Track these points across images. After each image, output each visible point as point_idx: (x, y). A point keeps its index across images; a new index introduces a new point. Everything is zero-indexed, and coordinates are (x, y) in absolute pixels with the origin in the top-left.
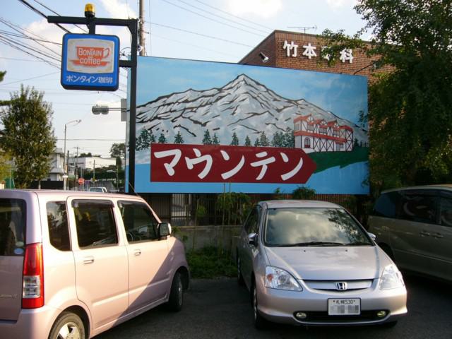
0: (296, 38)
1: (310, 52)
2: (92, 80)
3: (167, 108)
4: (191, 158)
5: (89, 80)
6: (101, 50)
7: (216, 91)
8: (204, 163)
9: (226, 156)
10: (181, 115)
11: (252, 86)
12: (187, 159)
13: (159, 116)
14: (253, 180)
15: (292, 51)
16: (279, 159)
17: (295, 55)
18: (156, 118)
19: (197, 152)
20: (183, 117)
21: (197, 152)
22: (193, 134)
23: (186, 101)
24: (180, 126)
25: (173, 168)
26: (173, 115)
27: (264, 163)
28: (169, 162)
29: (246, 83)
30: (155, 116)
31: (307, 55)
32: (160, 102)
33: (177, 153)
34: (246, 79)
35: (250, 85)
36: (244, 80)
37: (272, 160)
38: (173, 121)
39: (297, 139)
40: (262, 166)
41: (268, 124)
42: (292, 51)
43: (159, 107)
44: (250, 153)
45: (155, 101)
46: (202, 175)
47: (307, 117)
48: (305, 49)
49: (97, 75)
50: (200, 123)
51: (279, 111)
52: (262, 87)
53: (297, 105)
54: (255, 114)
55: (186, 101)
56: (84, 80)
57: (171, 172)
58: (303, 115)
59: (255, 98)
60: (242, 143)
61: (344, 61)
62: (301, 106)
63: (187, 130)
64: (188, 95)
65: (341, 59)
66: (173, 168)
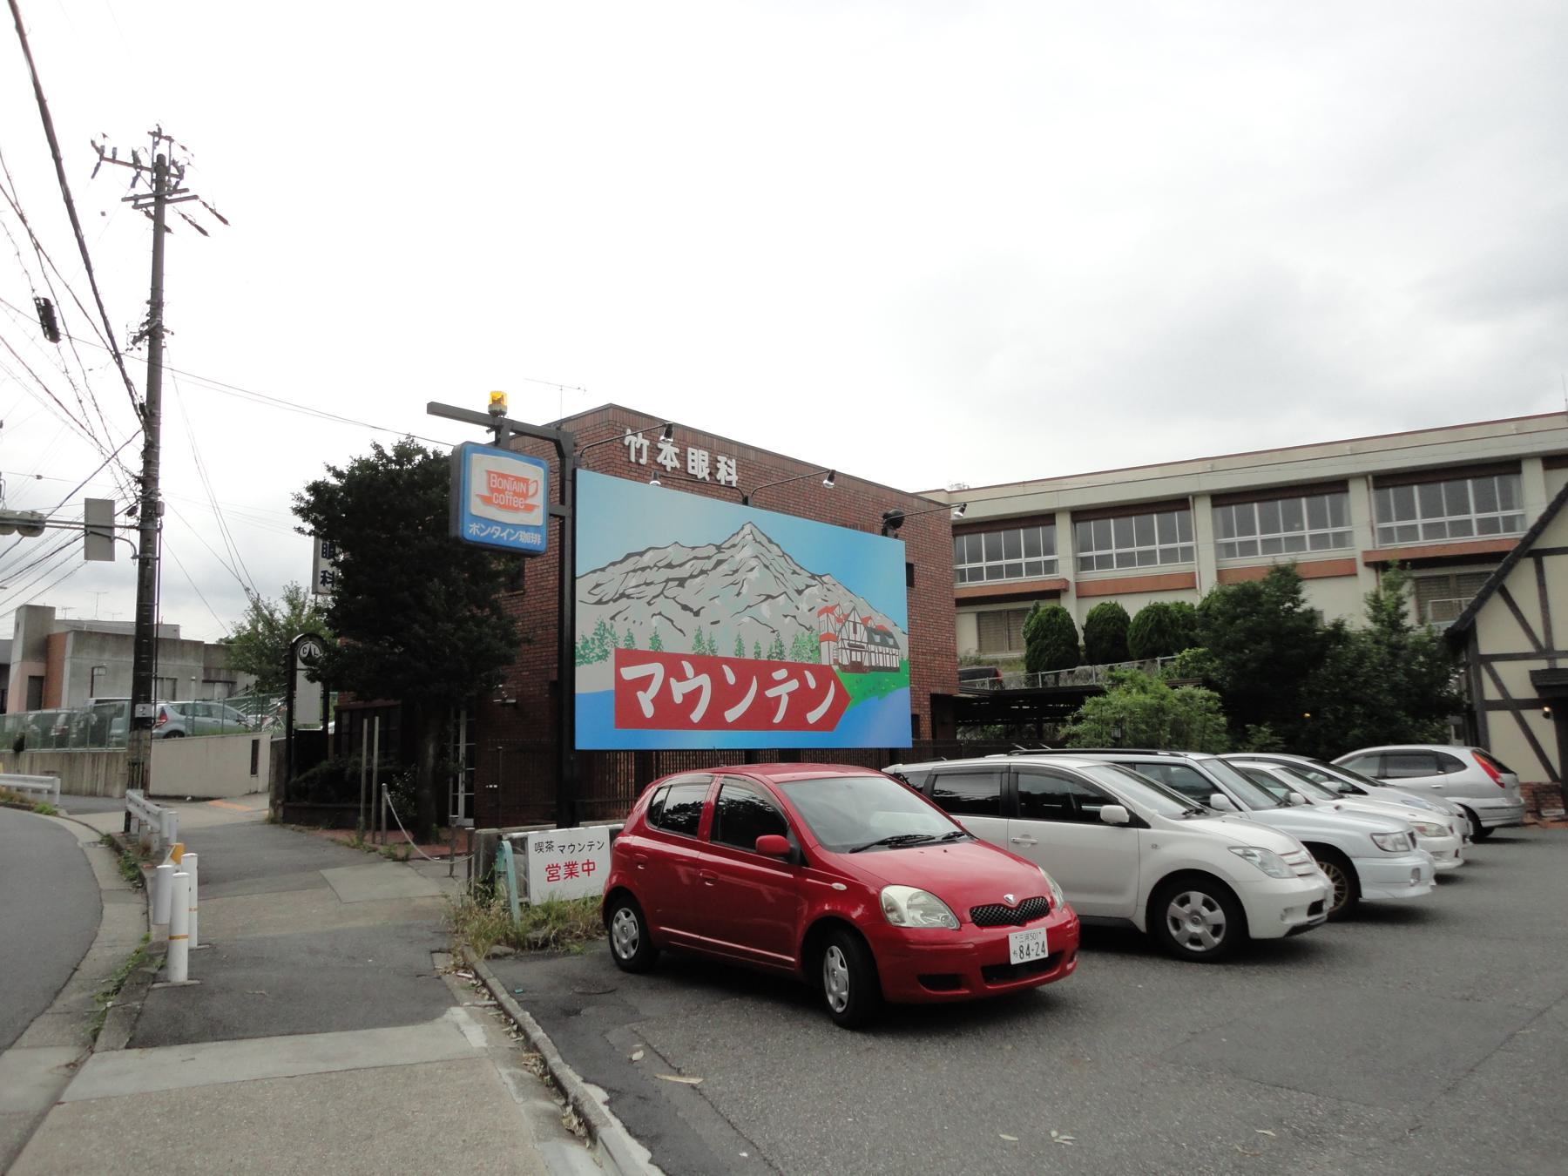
1: (669, 458)
2: (509, 535)
4: (679, 681)
5: (505, 534)
6: (525, 481)
9: (731, 678)
10: (662, 593)
12: (673, 681)
15: (639, 452)
16: (803, 681)
17: (643, 461)
18: (623, 595)
19: (688, 668)
20: (666, 597)
21: (688, 668)
22: (680, 630)
24: (660, 614)
28: (645, 689)
29: (755, 539)
31: (664, 463)
33: (657, 670)
34: (755, 530)
35: (760, 543)
40: (781, 696)
41: (786, 616)
42: (639, 452)
44: (762, 670)
46: (696, 716)
47: (834, 608)
48: (661, 450)
49: (516, 527)
50: (691, 610)
53: (823, 583)
54: (769, 597)
56: (498, 534)
57: (648, 711)
60: (749, 655)
62: (828, 586)
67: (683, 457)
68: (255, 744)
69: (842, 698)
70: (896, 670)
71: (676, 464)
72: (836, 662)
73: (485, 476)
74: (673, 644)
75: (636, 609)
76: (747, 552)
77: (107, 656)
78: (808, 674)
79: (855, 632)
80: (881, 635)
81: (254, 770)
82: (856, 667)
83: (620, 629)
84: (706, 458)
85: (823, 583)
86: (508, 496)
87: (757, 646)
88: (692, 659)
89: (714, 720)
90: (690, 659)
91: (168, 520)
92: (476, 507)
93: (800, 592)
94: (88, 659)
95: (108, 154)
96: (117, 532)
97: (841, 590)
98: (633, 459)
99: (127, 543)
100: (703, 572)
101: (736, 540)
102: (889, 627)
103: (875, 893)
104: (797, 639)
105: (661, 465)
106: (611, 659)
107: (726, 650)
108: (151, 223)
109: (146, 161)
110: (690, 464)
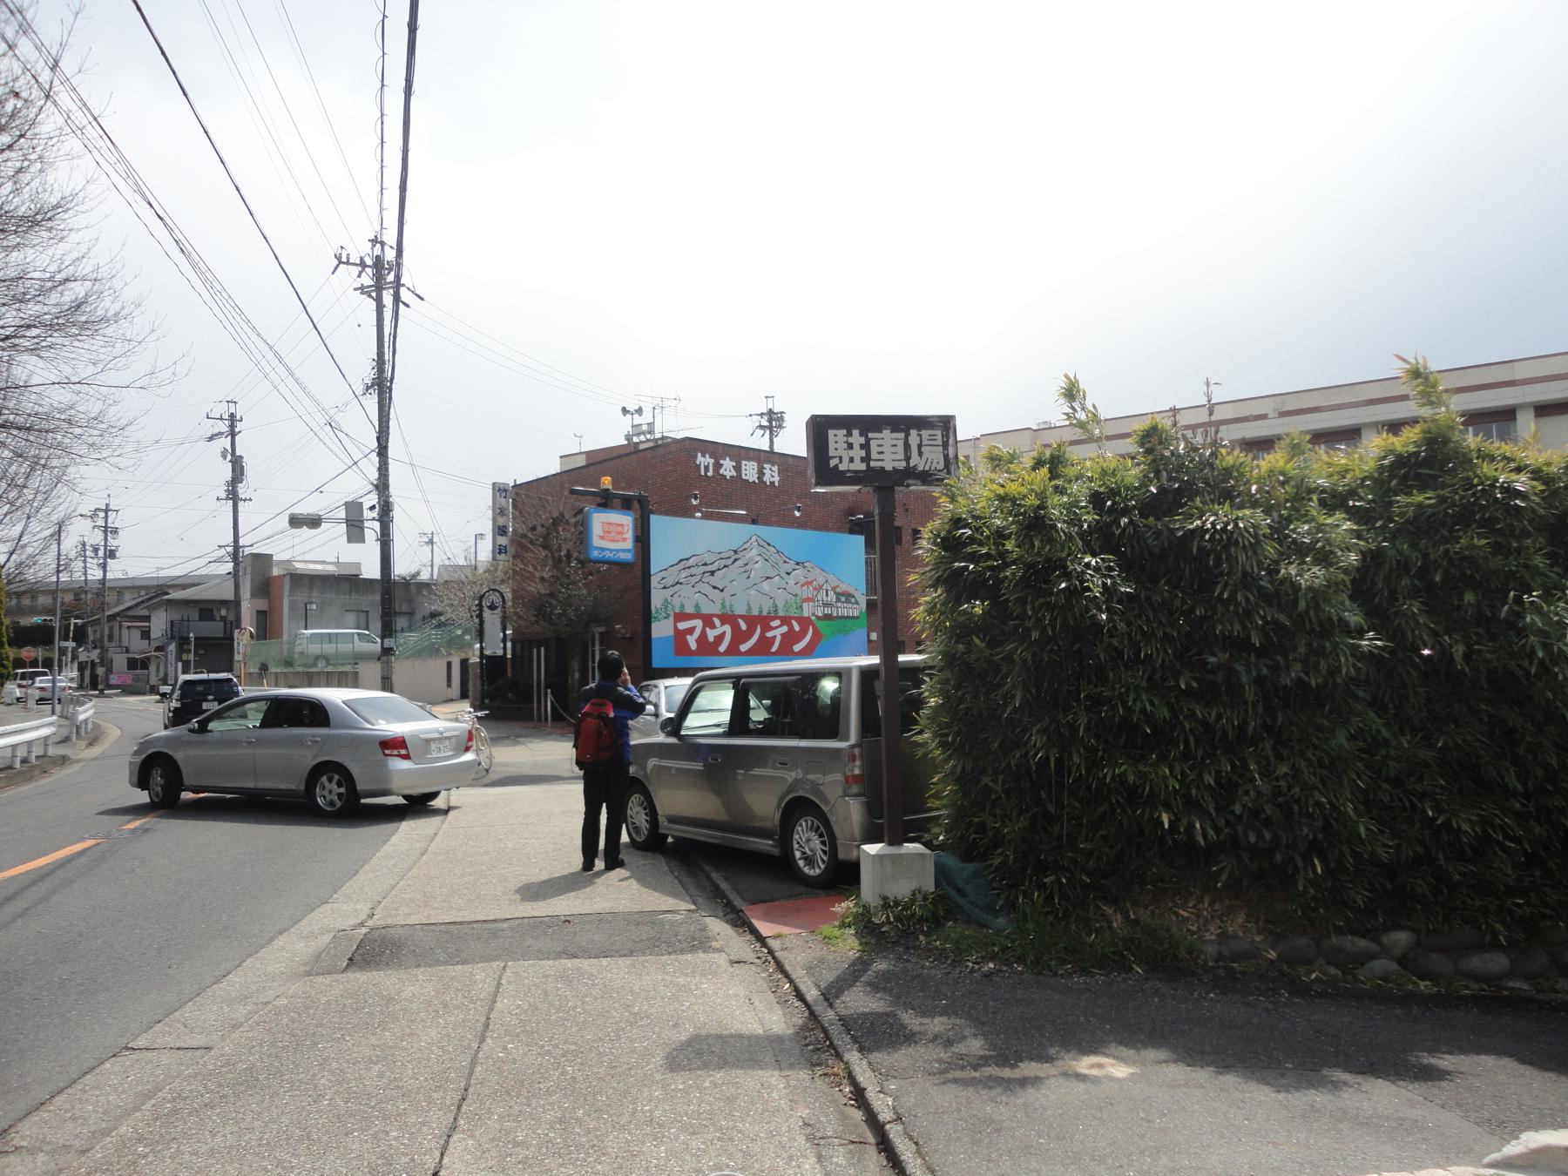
3: (688, 572)
6: (622, 525)
9: (743, 626)
12: (707, 629)
15: (707, 468)
18: (678, 583)
19: (717, 621)
21: (717, 621)
26: (694, 580)
28: (691, 634)
32: (681, 565)
33: (698, 623)
42: (707, 468)
44: (764, 621)
46: (722, 648)
49: (618, 551)
53: (804, 567)
54: (768, 578)
57: (693, 646)
60: (755, 612)
67: (738, 468)
68: (449, 664)
69: (817, 636)
70: (857, 617)
71: (734, 473)
72: (813, 614)
73: (600, 525)
74: (707, 609)
75: (685, 590)
76: (754, 552)
77: (315, 594)
78: (794, 622)
79: (827, 595)
80: (848, 597)
81: (449, 685)
82: (828, 617)
83: (676, 602)
84: (756, 468)
85: (804, 567)
86: (614, 535)
87: (760, 607)
88: (718, 616)
89: (733, 650)
90: (718, 616)
91: (397, 513)
92: (596, 542)
93: (788, 574)
94: (301, 598)
95: (344, 259)
96: (367, 524)
97: (817, 571)
98: (703, 473)
99: (372, 529)
100: (725, 566)
101: (746, 546)
102: (852, 591)
103: (399, 628)
104: (787, 602)
105: (723, 475)
106: (672, 618)
107: (740, 610)
108: (375, 303)
109: (369, 262)
110: (744, 472)
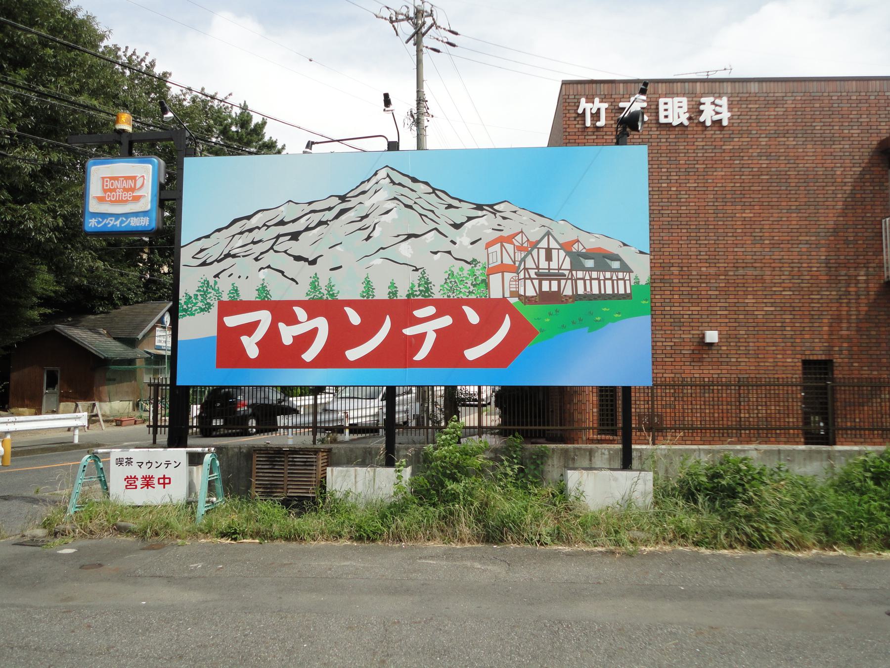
0: (604, 88)
2: (121, 223)
3: (248, 238)
4: (288, 324)
5: (118, 223)
6: (134, 178)
7: (337, 200)
8: (314, 331)
9: (355, 318)
10: (272, 248)
11: (404, 186)
12: (281, 325)
13: (232, 253)
14: (407, 362)
16: (459, 318)
17: (601, 123)
18: (228, 255)
19: (301, 313)
20: (276, 252)
21: (301, 313)
22: (292, 279)
23: (282, 223)
24: (269, 267)
25: (257, 344)
26: (258, 249)
27: (430, 330)
29: (392, 182)
30: (226, 252)
32: (236, 228)
33: (264, 317)
35: (400, 184)
36: (388, 176)
37: (446, 321)
38: (256, 259)
39: (495, 280)
41: (436, 253)
42: (596, 116)
43: (234, 236)
45: (226, 228)
46: (309, 356)
49: (127, 215)
50: (306, 260)
51: (457, 226)
52: (422, 186)
54: (410, 236)
55: (282, 223)
56: (112, 223)
57: (253, 352)
58: (505, 234)
59: (410, 207)
60: (381, 294)
61: (708, 123)
63: (282, 272)
64: (287, 213)
65: (702, 119)
66: (257, 344)
